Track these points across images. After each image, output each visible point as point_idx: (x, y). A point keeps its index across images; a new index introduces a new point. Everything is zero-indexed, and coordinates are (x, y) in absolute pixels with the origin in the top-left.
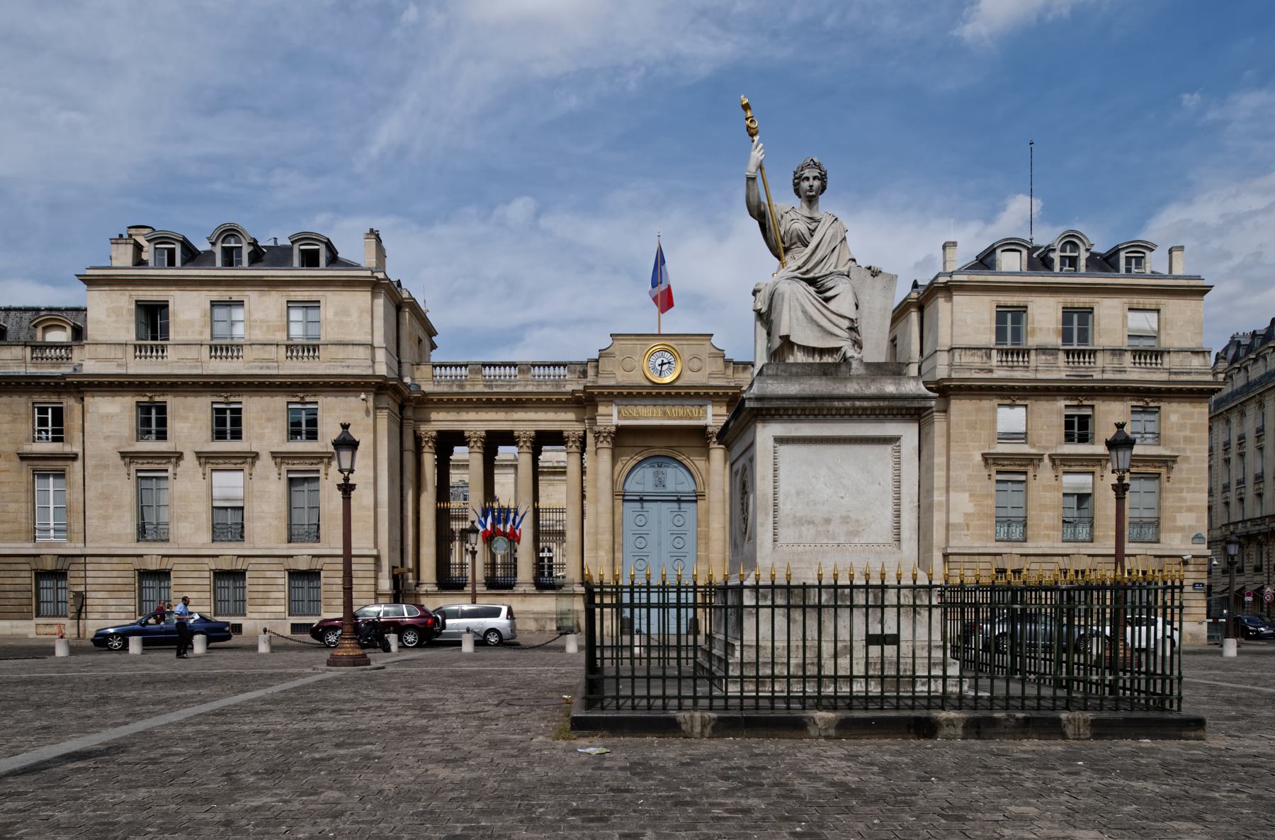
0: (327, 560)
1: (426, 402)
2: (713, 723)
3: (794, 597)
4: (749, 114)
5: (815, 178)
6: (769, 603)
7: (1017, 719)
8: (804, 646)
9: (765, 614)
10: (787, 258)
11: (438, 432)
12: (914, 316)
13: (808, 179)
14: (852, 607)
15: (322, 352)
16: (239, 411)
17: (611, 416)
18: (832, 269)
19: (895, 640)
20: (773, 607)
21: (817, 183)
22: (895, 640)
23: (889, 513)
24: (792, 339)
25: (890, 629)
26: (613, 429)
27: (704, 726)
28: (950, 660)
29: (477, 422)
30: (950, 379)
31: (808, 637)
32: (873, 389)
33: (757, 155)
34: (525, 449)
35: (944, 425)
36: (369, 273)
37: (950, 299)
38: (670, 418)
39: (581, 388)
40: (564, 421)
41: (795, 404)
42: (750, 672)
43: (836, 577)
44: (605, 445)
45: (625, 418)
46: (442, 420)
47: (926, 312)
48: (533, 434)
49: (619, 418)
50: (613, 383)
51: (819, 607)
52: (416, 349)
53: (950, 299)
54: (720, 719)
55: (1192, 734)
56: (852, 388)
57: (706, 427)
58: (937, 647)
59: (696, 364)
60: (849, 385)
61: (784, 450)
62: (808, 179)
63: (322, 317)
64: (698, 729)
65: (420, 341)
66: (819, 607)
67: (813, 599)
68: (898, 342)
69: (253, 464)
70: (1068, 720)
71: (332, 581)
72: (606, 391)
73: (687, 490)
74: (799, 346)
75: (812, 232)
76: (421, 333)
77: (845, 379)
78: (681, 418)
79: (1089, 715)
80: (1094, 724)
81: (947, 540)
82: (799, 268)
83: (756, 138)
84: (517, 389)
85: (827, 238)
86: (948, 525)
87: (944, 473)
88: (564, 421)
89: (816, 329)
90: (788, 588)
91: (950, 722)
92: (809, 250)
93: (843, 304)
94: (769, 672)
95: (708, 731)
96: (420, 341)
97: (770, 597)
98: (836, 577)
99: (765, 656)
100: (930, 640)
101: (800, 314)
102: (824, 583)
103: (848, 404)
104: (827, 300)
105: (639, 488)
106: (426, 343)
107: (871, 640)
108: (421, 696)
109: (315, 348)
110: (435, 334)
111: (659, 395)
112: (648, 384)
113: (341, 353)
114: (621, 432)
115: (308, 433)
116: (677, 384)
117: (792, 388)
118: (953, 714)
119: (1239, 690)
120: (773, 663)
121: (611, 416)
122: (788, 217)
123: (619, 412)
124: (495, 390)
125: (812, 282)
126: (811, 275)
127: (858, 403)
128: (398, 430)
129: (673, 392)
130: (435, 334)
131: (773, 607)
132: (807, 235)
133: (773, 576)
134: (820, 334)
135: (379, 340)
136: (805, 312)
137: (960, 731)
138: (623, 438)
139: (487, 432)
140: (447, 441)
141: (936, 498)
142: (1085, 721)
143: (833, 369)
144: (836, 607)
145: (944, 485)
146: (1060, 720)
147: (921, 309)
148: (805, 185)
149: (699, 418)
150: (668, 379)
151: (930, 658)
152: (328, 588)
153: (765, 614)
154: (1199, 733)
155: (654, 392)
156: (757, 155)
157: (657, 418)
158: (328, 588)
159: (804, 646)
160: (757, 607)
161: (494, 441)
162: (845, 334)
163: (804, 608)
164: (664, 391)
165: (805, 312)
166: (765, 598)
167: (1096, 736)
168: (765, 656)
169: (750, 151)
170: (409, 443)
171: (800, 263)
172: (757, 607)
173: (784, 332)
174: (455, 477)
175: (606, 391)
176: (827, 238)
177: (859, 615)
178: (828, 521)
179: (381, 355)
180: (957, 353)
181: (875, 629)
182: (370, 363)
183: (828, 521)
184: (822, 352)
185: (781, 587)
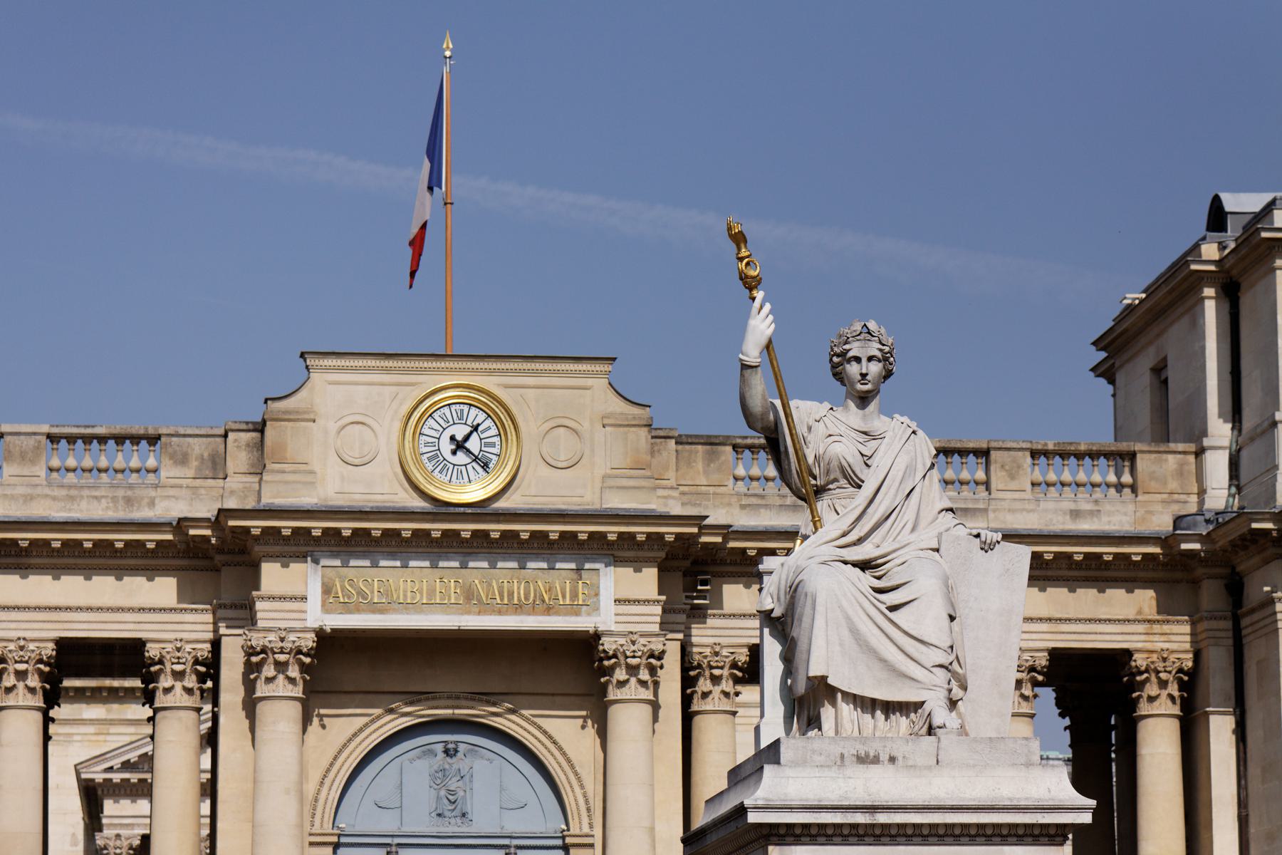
4: (744, 253)
10: (822, 505)
13: (858, 360)
17: (301, 600)
21: (875, 369)
24: (830, 681)
26: (309, 641)
33: (761, 326)
38: (484, 608)
39: (206, 510)
40: (146, 608)
44: (281, 687)
45: (347, 608)
47: (1246, 301)
48: (49, 650)
49: (326, 608)
50: (307, 499)
57: (597, 636)
59: (565, 446)
62: (858, 360)
68: (1172, 374)
72: (286, 525)
73: (537, 826)
74: (846, 695)
75: (867, 460)
78: (519, 609)
83: (759, 295)
85: (897, 473)
88: (146, 608)
93: (926, 618)
101: (845, 633)
105: (386, 823)
111: (450, 545)
112: (418, 503)
114: (332, 645)
116: (501, 504)
121: (301, 600)
122: (820, 429)
123: (327, 590)
125: (864, 566)
126: (865, 552)
129: (495, 529)
136: (855, 632)
138: (342, 666)
147: (1231, 292)
148: (853, 370)
149: (574, 610)
150: (474, 490)
155: (436, 528)
156: (761, 326)
157: (444, 607)
164: (466, 528)
169: (747, 316)
173: (815, 671)
175: (286, 525)
176: (897, 473)
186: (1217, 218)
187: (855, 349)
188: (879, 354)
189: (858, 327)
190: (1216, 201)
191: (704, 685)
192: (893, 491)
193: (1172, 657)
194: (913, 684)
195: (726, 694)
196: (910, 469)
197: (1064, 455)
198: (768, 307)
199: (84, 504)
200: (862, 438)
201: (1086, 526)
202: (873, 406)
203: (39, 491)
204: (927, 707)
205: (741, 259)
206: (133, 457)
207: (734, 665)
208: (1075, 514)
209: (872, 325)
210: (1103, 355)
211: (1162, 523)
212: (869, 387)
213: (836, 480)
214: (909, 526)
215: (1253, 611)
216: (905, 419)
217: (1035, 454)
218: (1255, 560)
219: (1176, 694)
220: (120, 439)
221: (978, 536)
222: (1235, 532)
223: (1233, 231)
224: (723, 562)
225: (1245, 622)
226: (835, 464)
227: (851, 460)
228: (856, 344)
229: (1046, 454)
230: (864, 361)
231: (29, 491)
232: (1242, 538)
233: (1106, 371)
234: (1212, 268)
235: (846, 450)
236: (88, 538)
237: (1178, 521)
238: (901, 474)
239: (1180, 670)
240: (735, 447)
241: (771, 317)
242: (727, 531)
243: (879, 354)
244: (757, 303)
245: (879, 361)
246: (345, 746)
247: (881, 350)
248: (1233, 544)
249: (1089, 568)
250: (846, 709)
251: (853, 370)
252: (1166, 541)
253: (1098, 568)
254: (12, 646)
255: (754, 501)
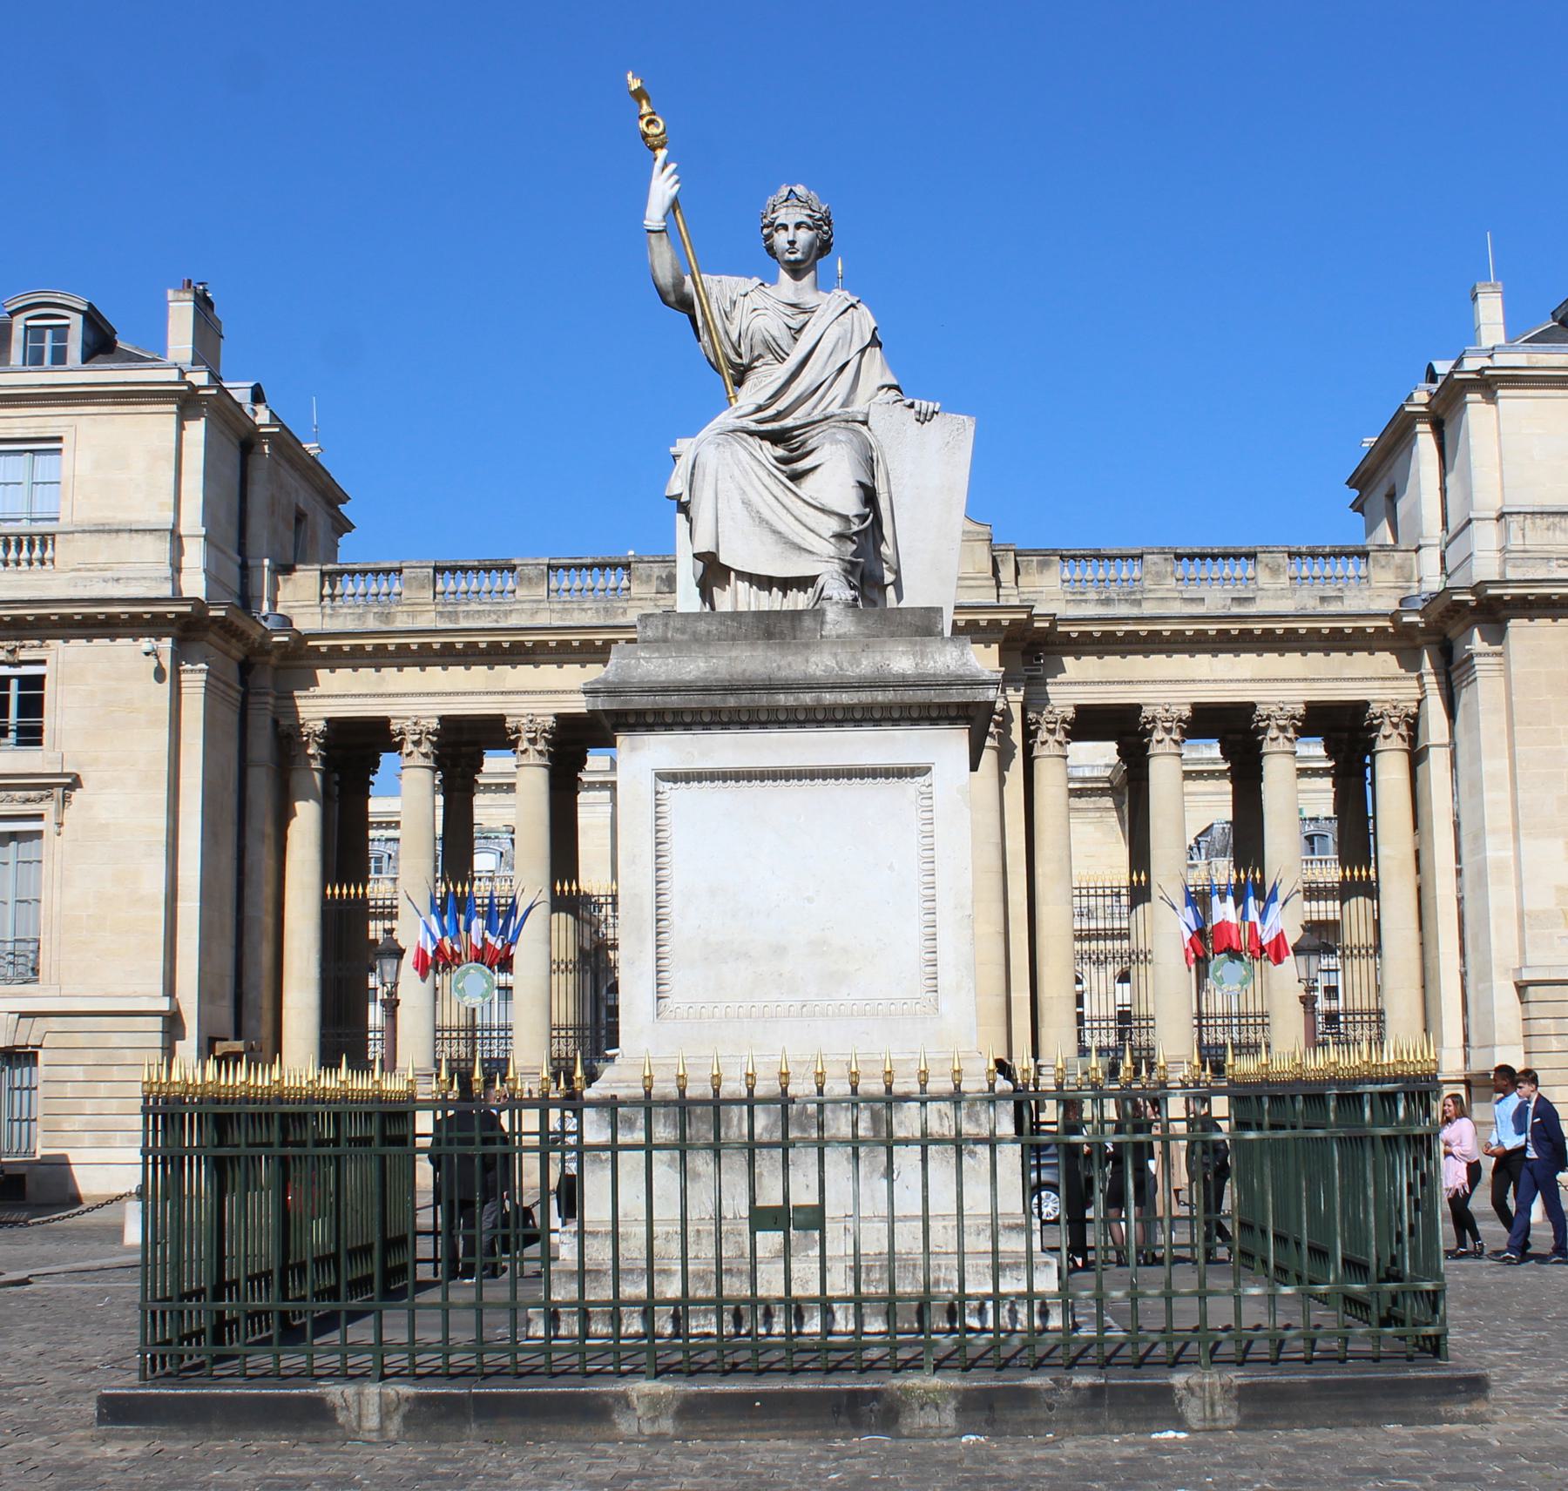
0: (55, 1023)
1: (303, 658)
2: (405, 1408)
3: (694, 1120)
5: (798, 226)
6: (639, 1137)
7: (1077, 1389)
8: (719, 1231)
9: (631, 1162)
11: (329, 721)
12: (1425, 441)
13: (785, 227)
14: (821, 1145)
15: (62, 551)
16: (37, 682)
18: (834, 409)
19: (762, 1218)
20: (649, 1147)
21: (804, 236)
22: (815, 1218)
23: (914, 932)
25: (802, 1195)
27: (385, 1413)
28: (1040, 1257)
29: (417, 698)
30: (1504, 583)
31: (692, 1214)
32: (865, 666)
33: (663, 187)
34: (532, 757)
35: (1500, 684)
36: (173, 375)
37: (1491, 398)
41: (694, 701)
42: (600, 1292)
43: (717, 1080)
46: (330, 698)
51: (751, 1147)
52: (289, 536)
53: (1491, 398)
54: (421, 1400)
55: (1462, 1410)
56: (819, 664)
58: (1011, 1228)
60: (813, 659)
61: (677, 795)
62: (785, 227)
63: (66, 471)
64: (372, 1421)
65: (300, 517)
66: (751, 1147)
67: (736, 1125)
69: (65, 799)
70: (1189, 1388)
71: (62, 1073)
74: (742, 575)
76: (304, 497)
77: (807, 646)
79: (1236, 1377)
80: (1245, 1395)
81: (1523, 952)
82: (760, 409)
83: (662, 154)
84: (513, 622)
86: (1521, 915)
87: (1506, 795)
89: (770, 538)
90: (683, 1106)
91: (929, 1401)
92: (782, 371)
94: (641, 1290)
95: (395, 1425)
96: (300, 517)
97: (641, 1122)
98: (717, 1080)
99: (633, 1249)
100: (995, 1215)
102: (758, 1092)
103: (808, 698)
104: (796, 477)
106: (319, 519)
107: (762, 1218)
108: (76, 1348)
109: (46, 539)
110: (345, 498)
113: (103, 550)
115: (21, 731)
117: (692, 667)
118: (936, 1381)
119: (280, 1377)
120: (650, 1272)
124: (464, 624)
125: (776, 438)
126: (789, 422)
127: (828, 698)
128: (234, 718)
130: (345, 498)
131: (649, 1147)
132: (784, 339)
133: (751, 1077)
134: (778, 549)
135: (192, 521)
137: (950, 1418)
139: (443, 719)
140: (359, 746)
141: (1490, 854)
142: (1226, 1389)
143: (786, 624)
144: (785, 1145)
145: (1508, 822)
146: (1170, 1388)
147: (1438, 428)
151: (995, 1252)
152: (54, 1090)
153: (631, 1162)
154: (1478, 1407)
156: (663, 187)
158: (54, 1090)
159: (719, 1231)
160: (614, 1148)
161: (462, 747)
162: (829, 548)
163: (717, 1149)
165: (747, 503)
166: (631, 1125)
167: (1250, 1422)
168: (633, 1249)
170: (262, 747)
171: (761, 399)
172: (614, 1148)
174: (487, 811)
177: (735, 1164)
178: (779, 951)
179: (195, 555)
180: (1514, 523)
181: (771, 1196)
182: (168, 572)
183: (779, 951)
184: (786, 584)
185: (665, 1103)
186: (1432, 376)
187: (783, 216)
188: (809, 221)
189: (784, 191)
190: (1430, 366)
191: (1042, 735)
192: (820, 363)
193: (1401, 705)
194: (807, 555)
195: (1060, 743)
196: (844, 340)
197: (1313, 555)
198: (673, 166)
199: (576, 614)
200: (790, 311)
201: (1333, 608)
202: (808, 279)
203: (542, 606)
204: (820, 581)
205: (641, 117)
206: (613, 579)
207: (1064, 721)
208: (1323, 599)
209: (800, 190)
210: (1356, 493)
211: (1390, 605)
212: (799, 256)
213: (760, 356)
214: (839, 401)
215: (1459, 667)
216: (846, 294)
217: (1291, 555)
218: (1461, 627)
219: (1405, 733)
220: (602, 566)
221: (911, 406)
222: (1440, 606)
223: (1440, 380)
224: (1054, 644)
225: (1454, 676)
226: (758, 338)
227: (776, 334)
228: (783, 211)
229: (1300, 555)
230: (791, 228)
231: (535, 605)
232: (1447, 610)
233: (1358, 507)
234: (1423, 409)
235: (772, 324)
236: (575, 638)
237: (1402, 602)
238: (831, 346)
239: (1407, 715)
240: (1062, 557)
241: (675, 177)
242: (1054, 620)
243: (809, 221)
244: (659, 164)
245: (810, 228)
246: (420, 694)
247: (810, 216)
248: (1441, 615)
249: (1334, 640)
250: (743, 586)
251: (781, 239)
252: (1394, 617)
253: (1341, 640)
254: (524, 721)
255: (1079, 597)
